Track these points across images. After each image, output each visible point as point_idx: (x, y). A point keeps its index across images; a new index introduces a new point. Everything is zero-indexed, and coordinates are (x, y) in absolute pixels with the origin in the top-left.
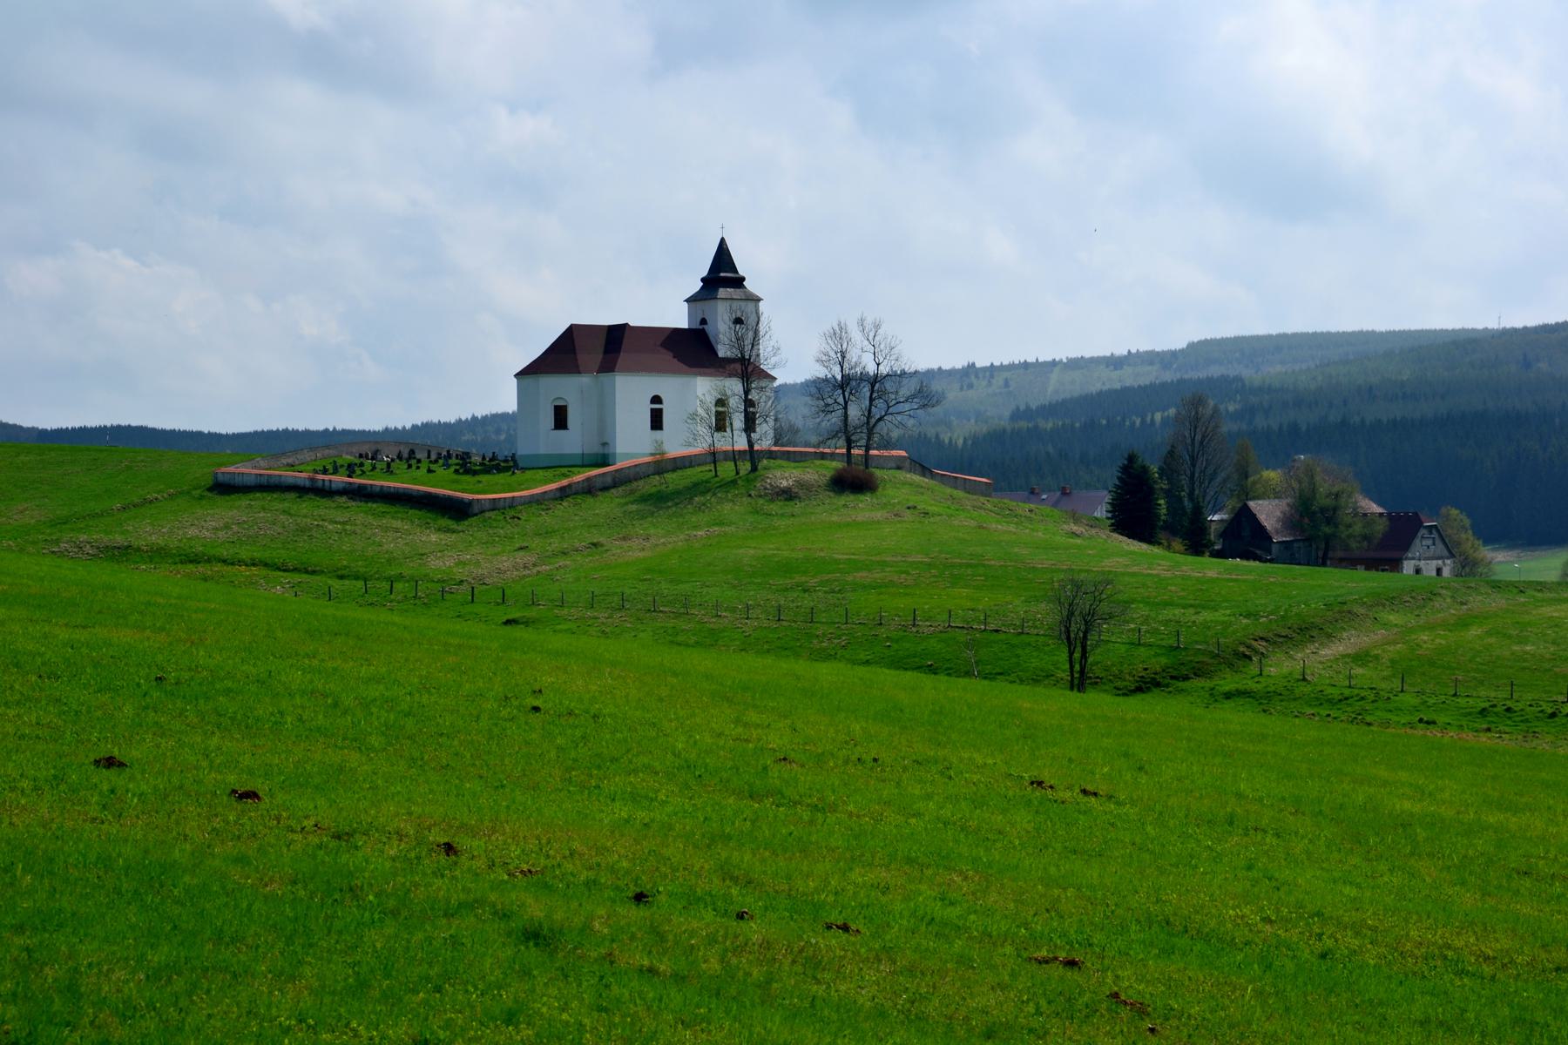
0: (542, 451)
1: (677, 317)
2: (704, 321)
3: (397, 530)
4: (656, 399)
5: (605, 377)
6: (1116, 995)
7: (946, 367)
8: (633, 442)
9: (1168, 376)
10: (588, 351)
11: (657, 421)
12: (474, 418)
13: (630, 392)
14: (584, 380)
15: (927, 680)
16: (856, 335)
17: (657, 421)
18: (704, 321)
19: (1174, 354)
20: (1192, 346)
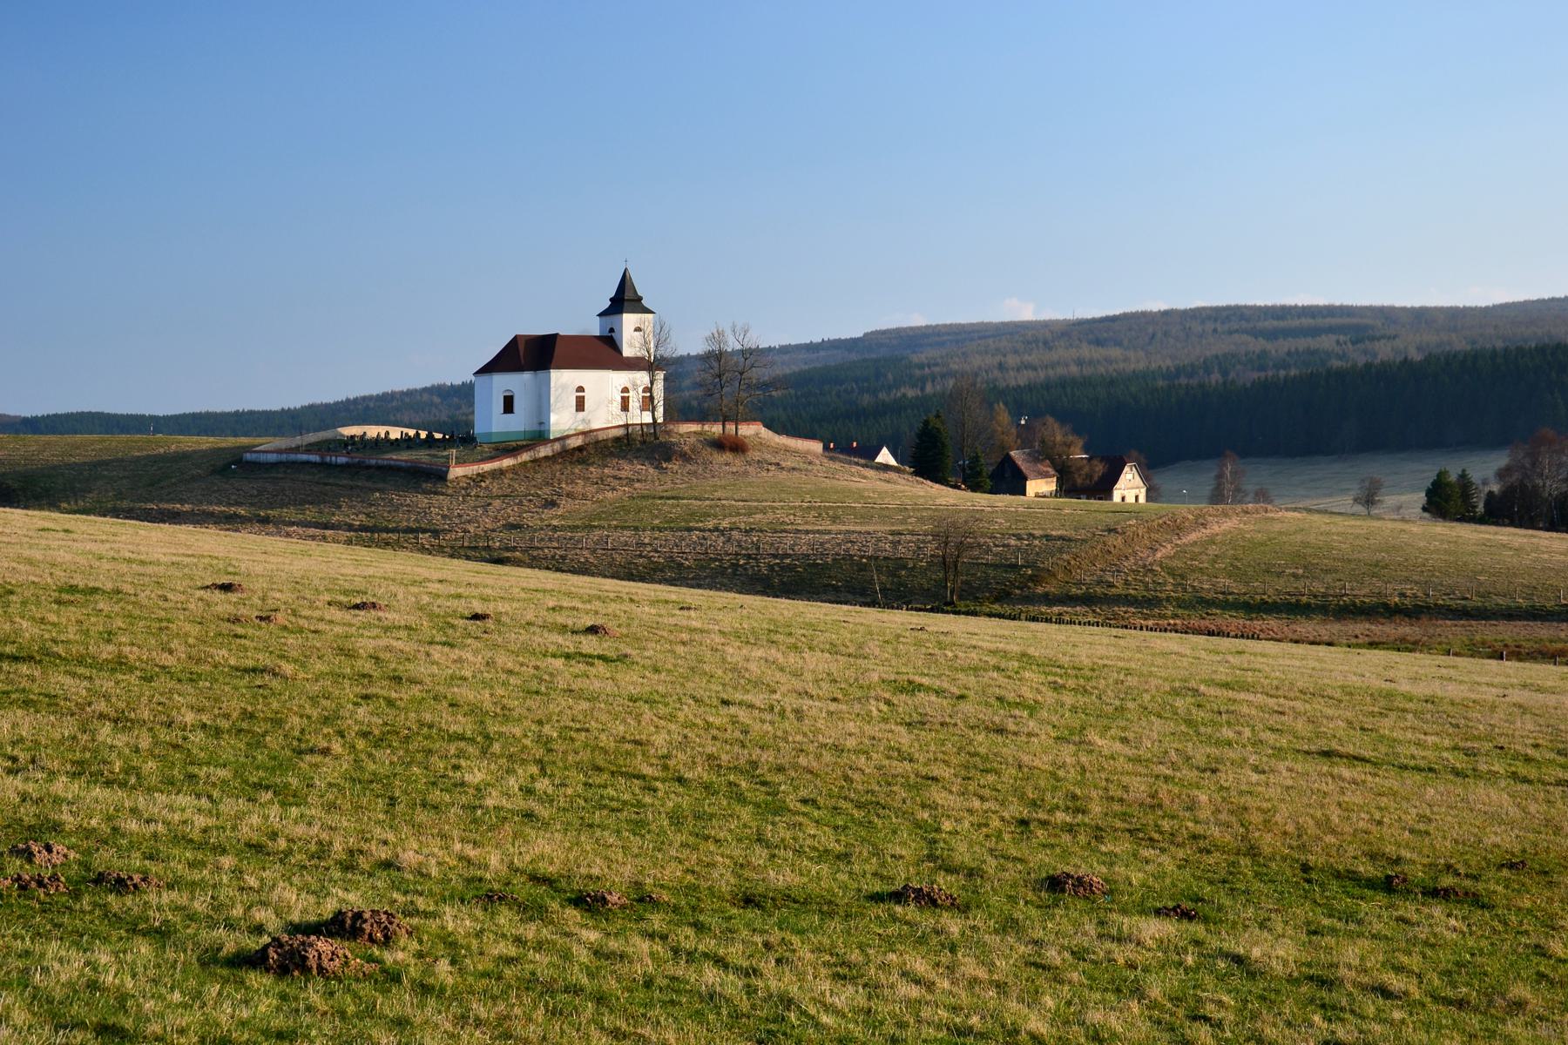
0: (494, 430)
1: (594, 328)
2: (612, 330)
3: (362, 488)
4: (581, 389)
5: (541, 374)
6: (1214, 771)
7: (693, 353)
8: (562, 420)
9: (854, 357)
10: (534, 354)
11: (580, 405)
12: (348, 400)
13: (563, 380)
14: (527, 376)
15: (1493, 664)
16: (728, 333)
17: (580, 405)
18: (612, 330)
19: (854, 341)
20: (866, 335)
